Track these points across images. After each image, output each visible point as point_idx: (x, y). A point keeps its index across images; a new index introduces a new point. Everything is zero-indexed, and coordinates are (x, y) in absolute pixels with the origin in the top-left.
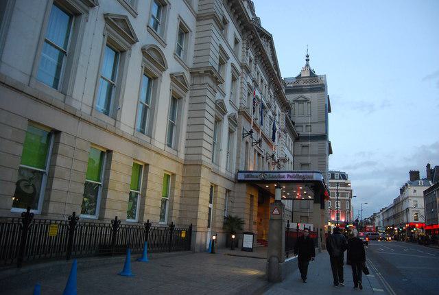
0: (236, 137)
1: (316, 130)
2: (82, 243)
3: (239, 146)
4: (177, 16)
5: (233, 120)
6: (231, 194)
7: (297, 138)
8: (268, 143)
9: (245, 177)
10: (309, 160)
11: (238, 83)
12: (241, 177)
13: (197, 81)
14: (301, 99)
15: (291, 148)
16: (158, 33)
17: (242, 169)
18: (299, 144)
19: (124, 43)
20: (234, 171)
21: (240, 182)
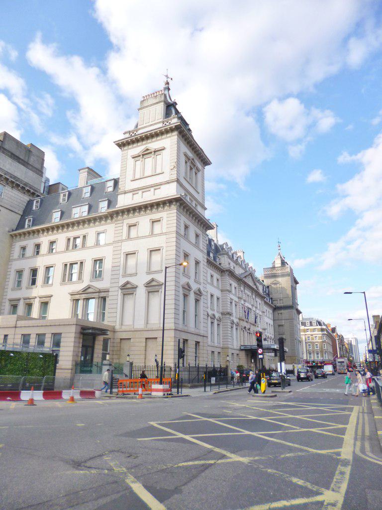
0: (238, 330)
1: (290, 303)
2: (151, 390)
3: (240, 334)
4: (194, 259)
5: (237, 325)
6: (221, 354)
7: (275, 309)
8: (254, 325)
9: (353, 408)
10: (283, 322)
11: (238, 306)
12: (242, 348)
13: (224, 316)
14: (275, 282)
15: (271, 316)
16: (186, 273)
17: (242, 344)
18: (276, 313)
19: (313, 406)
20: (239, 345)
21: (242, 350)
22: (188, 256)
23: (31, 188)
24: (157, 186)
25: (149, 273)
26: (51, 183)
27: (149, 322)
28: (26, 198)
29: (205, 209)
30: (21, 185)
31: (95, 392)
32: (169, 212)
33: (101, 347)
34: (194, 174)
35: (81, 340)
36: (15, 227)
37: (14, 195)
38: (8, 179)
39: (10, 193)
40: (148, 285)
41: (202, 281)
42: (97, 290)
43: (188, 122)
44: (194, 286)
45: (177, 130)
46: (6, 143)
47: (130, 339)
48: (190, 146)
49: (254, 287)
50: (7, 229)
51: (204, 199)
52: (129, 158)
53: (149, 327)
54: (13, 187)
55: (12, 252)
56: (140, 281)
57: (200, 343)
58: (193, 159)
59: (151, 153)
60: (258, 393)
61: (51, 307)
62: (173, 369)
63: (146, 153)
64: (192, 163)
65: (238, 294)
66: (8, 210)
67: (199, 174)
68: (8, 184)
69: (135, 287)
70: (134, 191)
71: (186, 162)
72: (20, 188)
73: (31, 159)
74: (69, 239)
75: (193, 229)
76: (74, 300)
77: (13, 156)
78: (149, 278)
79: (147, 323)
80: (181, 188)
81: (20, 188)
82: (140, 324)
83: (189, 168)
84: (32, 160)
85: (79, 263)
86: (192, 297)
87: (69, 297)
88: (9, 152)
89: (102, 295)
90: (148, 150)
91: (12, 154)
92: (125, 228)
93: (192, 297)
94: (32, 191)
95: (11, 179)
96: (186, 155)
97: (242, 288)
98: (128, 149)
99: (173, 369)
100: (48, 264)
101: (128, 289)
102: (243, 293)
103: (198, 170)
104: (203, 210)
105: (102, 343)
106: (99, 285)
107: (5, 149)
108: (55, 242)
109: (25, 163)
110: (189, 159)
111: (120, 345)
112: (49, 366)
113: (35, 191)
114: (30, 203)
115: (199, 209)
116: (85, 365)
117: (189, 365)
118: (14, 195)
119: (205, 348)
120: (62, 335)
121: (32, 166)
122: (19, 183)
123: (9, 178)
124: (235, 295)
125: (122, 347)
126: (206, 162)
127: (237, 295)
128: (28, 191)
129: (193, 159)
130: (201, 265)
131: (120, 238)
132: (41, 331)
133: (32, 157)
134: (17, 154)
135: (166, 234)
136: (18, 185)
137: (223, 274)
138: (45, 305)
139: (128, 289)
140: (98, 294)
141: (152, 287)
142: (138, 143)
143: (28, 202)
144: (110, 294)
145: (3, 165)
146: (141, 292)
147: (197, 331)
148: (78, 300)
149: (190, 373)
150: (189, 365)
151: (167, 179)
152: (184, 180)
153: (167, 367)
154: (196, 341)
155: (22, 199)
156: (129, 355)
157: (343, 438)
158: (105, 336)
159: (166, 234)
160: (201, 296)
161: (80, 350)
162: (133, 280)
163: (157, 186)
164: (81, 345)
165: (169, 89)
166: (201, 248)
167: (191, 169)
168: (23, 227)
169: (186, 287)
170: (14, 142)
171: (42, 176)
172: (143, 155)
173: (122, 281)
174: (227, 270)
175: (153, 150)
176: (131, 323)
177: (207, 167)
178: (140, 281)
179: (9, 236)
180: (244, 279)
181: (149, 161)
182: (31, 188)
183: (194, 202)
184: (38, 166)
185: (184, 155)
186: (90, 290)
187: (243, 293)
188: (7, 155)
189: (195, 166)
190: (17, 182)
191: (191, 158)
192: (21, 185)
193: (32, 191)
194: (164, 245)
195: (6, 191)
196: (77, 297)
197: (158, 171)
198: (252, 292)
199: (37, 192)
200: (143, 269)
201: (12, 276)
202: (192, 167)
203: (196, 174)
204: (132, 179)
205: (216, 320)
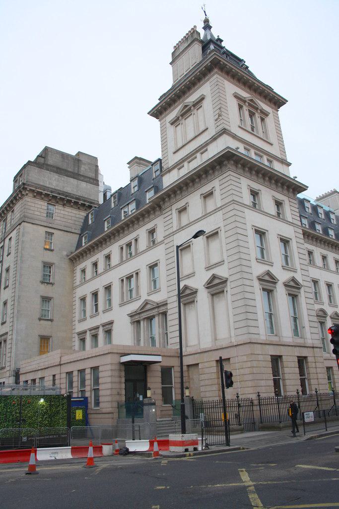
16: (266, 259)
22: (289, 241)
23: (85, 201)
24: (203, 148)
25: (208, 268)
26: (113, 191)
27: (218, 337)
28: (83, 214)
29: (289, 164)
30: (73, 200)
31: (102, 447)
32: (221, 178)
33: (160, 380)
34: (259, 120)
35: (123, 374)
36: (74, 249)
37: (67, 213)
38: (57, 197)
39: (62, 212)
41: (298, 267)
42: (155, 305)
43: (241, 58)
44: (283, 276)
45: (216, 67)
46: (49, 158)
47: (198, 364)
50: (65, 253)
51: (283, 151)
52: (168, 125)
53: (220, 344)
54: (64, 205)
55: (74, 278)
56: (198, 282)
57: (283, 357)
59: (190, 108)
61: (114, 333)
62: (256, 402)
63: (186, 112)
64: (250, 105)
66: (63, 232)
67: (269, 120)
68: (57, 202)
69: (195, 292)
72: (72, 204)
73: (82, 169)
74: (122, 248)
76: (134, 322)
77: (59, 171)
78: (209, 274)
79: (216, 339)
80: (235, 141)
81: (43, 196)
82: (207, 343)
83: (247, 114)
84: (84, 170)
85: (134, 275)
86: (281, 293)
87: (128, 319)
88: (54, 167)
89: (162, 309)
90: (186, 106)
91: (58, 168)
92: (175, 214)
93: (281, 293)
94: (87, 204)
95: (59, 196)
96: (236, 96)
98: (166, 116)
99: (256, 402)
100: (106, 283)
101: (186, 297)
103: (265, 114)
104: (285, 167)
105: (160, 374)
106: (157, 298)
107: (49, 165)
108: (156, 265)
109: (76, 176)
110: (245, 102)
111: (189, 374)
112: (58, 412)
113: (91, 203)
114: (87, 218)
115: (277, 167)
116: (133, 406)
117: (316, 392)
118: (67, 213)
119: (318, 365)
120: (101, 369)
121: (83, 176)
122: (69, 199)
123: (56, 195)
125: (191, 377)
126: (278, 102)
128: (83, 205)
129: (251, 100)
130: (294, 244)
131: (171, 231)
132: (80, 366)
133: (83, 166)
134: (64, 167)
136: (69, 202)
138: (109, 332)
140: (156, 310)
142: (174, 103)
143: (85, 217)
144: (169, 306)
145: (49, 182)
146: (203, 297)
147: (299, 341)
148: (138, 322)
149: (263, 407)
150: (316, 392)
152: (240, 129)
153: (245, 400)
154: (298, 357)
155: (77, 216)
160: (299, 288)
161: (123, 386)
162: (190, 283)
163: (203, 148)
164: (123, 380)
165: (210, 28)
166: (290, 220)
167: (252, 115)
168: (81, 246)
169: (292, 284)
170: (58, 156)
171: (98, 185)
172: (182, 116)
175: (191, 104)
176: (196, 343)
178: (198, 282)
179: (68, 261)
181: (190, 122)
182: (85, 201)
183: (265, 157)
184: (92, 175)
186: (148, 307)
188: (51, 171)
189: (257, 109)
190: (68, 198)
191: (247, 99)
192: (73, 200)
193: (87, 204)
194: (221, 225)
195: (57, 211)
196: (137, 318)
197: (202, 128)
199: (94, 203)
200: (201, 265)
201: (78, 303)
202: (242, 104)
203: (262, 120)
204: (174, 150)
205: (328, 318)
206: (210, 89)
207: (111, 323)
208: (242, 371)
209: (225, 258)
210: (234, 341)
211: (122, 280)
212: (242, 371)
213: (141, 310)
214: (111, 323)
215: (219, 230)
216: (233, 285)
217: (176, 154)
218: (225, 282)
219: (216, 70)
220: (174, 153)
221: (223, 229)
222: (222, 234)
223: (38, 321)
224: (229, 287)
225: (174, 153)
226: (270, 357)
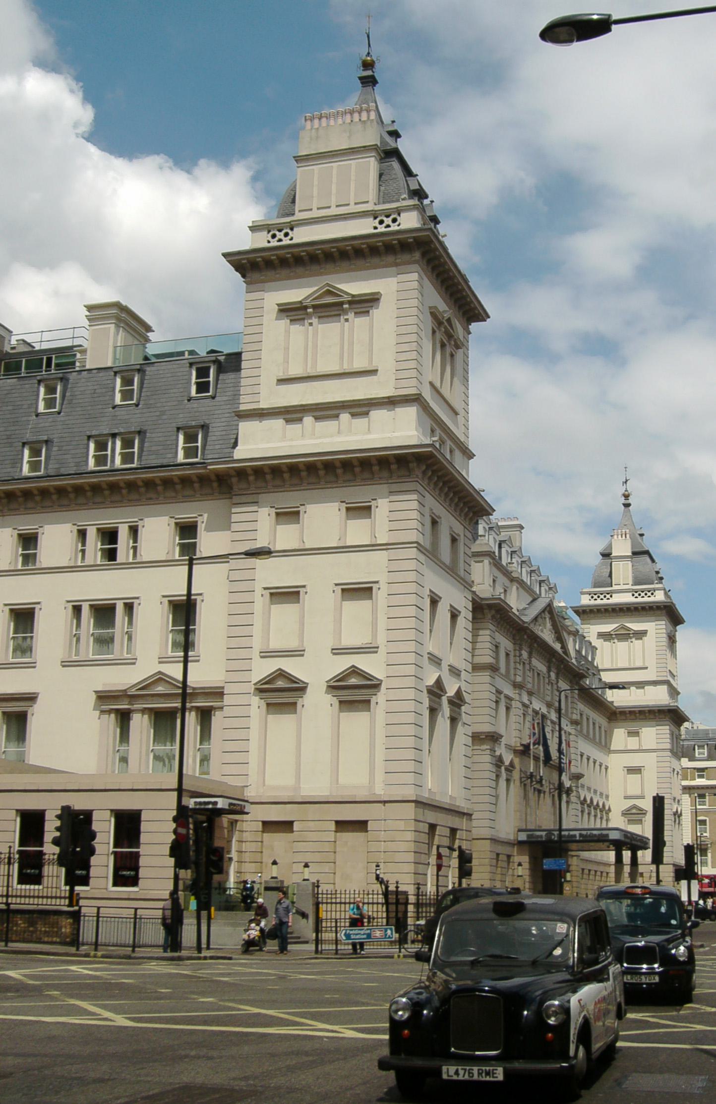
12: (523, 837)
40: (337, 686)
47: (291, 823)
48: (434, 269)
49: (557, 647)
56: (317, 670)
58: (449, 320)
60: (120, 761)
63: (330, 308)
65: (512, 672)
67: (460, 354)
70: (292, 414)
71: (434, 332)
75: (450, 522)
78: (343, 663)
83: (438, 345)
97: (525, 654)
102: (527, 667)
120: (244, 356)
124: (506, 676)
127: (512, 677)
135: (386, 547)
137: (480, 616)
139: (282, 693)
141: (354, 691)
151: (388, 391)
156: (275, 863)
157: (41, 852)
158: (623, 1004)
159: (386, 547)
163: (360, 408)
173: (263, 669)
174: (490, 606)
175: (346, 298)
177: (474, 327)
180: (531, 626)
183: (449, 443)
185: (431, 313)
187: (527, 667)
198: (549, 661)
203: (452, 356)
206: (395, 289)
207: (31, 698)
208: (392, 846)
209: (381, 640)
210: (380, 791)
211: (77, 610)
212: (392, 846)
213: (337, 681)
214: (31, 698)
215: (375, 586)
216: (392, 695)
217: (284, 388)
218: (375, 686)
219: (417, 255)
220: (281, 381)
221: (383, 585)
222: (381, 595)
223: (681, 792)
224: (380, 699)
225: (281, 381)
226: (427, 825)
